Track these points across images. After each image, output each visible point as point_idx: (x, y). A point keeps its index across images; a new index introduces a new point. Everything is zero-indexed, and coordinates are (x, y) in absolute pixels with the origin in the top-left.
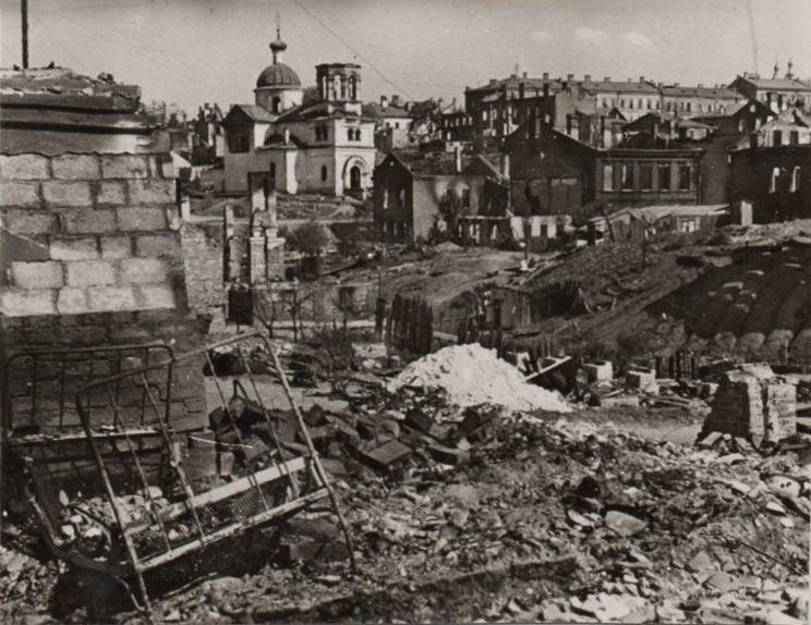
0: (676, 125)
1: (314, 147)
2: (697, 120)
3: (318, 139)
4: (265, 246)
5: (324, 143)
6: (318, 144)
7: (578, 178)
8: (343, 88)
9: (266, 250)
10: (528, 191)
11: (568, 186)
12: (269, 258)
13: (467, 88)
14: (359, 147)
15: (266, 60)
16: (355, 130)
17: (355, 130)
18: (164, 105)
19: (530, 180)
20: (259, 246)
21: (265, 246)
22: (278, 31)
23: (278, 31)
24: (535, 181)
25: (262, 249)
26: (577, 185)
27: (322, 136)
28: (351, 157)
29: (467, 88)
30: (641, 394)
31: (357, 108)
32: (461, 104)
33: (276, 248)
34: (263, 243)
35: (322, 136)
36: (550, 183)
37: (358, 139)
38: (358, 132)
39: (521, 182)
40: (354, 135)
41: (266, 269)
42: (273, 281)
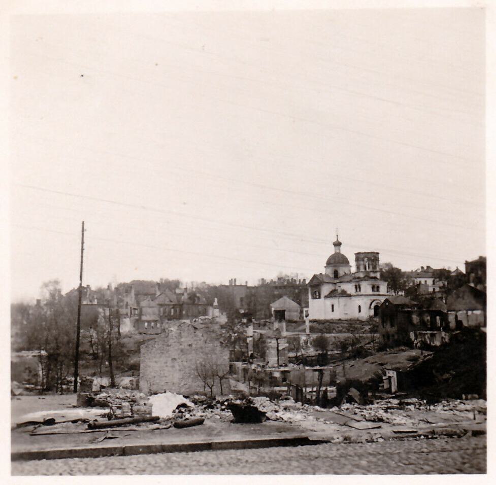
0: (267, 322)
1: (354, 296)
2: (192, 326)
3: (356, 291)
4: (278, 348)
5: (359, 293)
6: (356, 294)
7: (481, 310)
8: (369, 265)
9: (278, 350)
10: (456, 316)
11: (477, 315)
12: (279, 354)
13: (466, 261)
14: (379, 295)
15: (332, 251)
16: (376, 286)
17: (376, 286)
18: (297, 274)
19: (457, 311)
20: (274, 348)
21: (278, 348)
22: (337, 236)
23: (337, 236)
24: (460, 312)
25: (276, 350)
26: (481, 314)
27: (358, 290)
28: (374, 300)
29: (466, 261)
30: (437, 436)
31: (378, 275)
32: (463, 270)
33: (284, 349)
34: (277, 346)
35: (358, 290)
36: (467, 313)
37: (378, 290)
38: (378, 287)
39: (453, 312)
40: (376, 289)
41: (278, 360)
42: (281, 366)
